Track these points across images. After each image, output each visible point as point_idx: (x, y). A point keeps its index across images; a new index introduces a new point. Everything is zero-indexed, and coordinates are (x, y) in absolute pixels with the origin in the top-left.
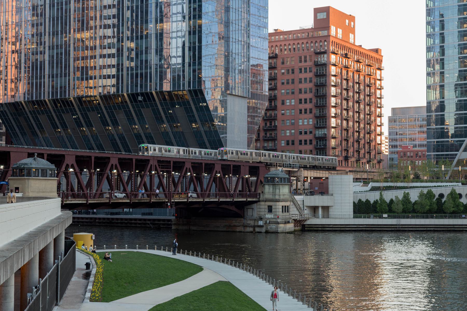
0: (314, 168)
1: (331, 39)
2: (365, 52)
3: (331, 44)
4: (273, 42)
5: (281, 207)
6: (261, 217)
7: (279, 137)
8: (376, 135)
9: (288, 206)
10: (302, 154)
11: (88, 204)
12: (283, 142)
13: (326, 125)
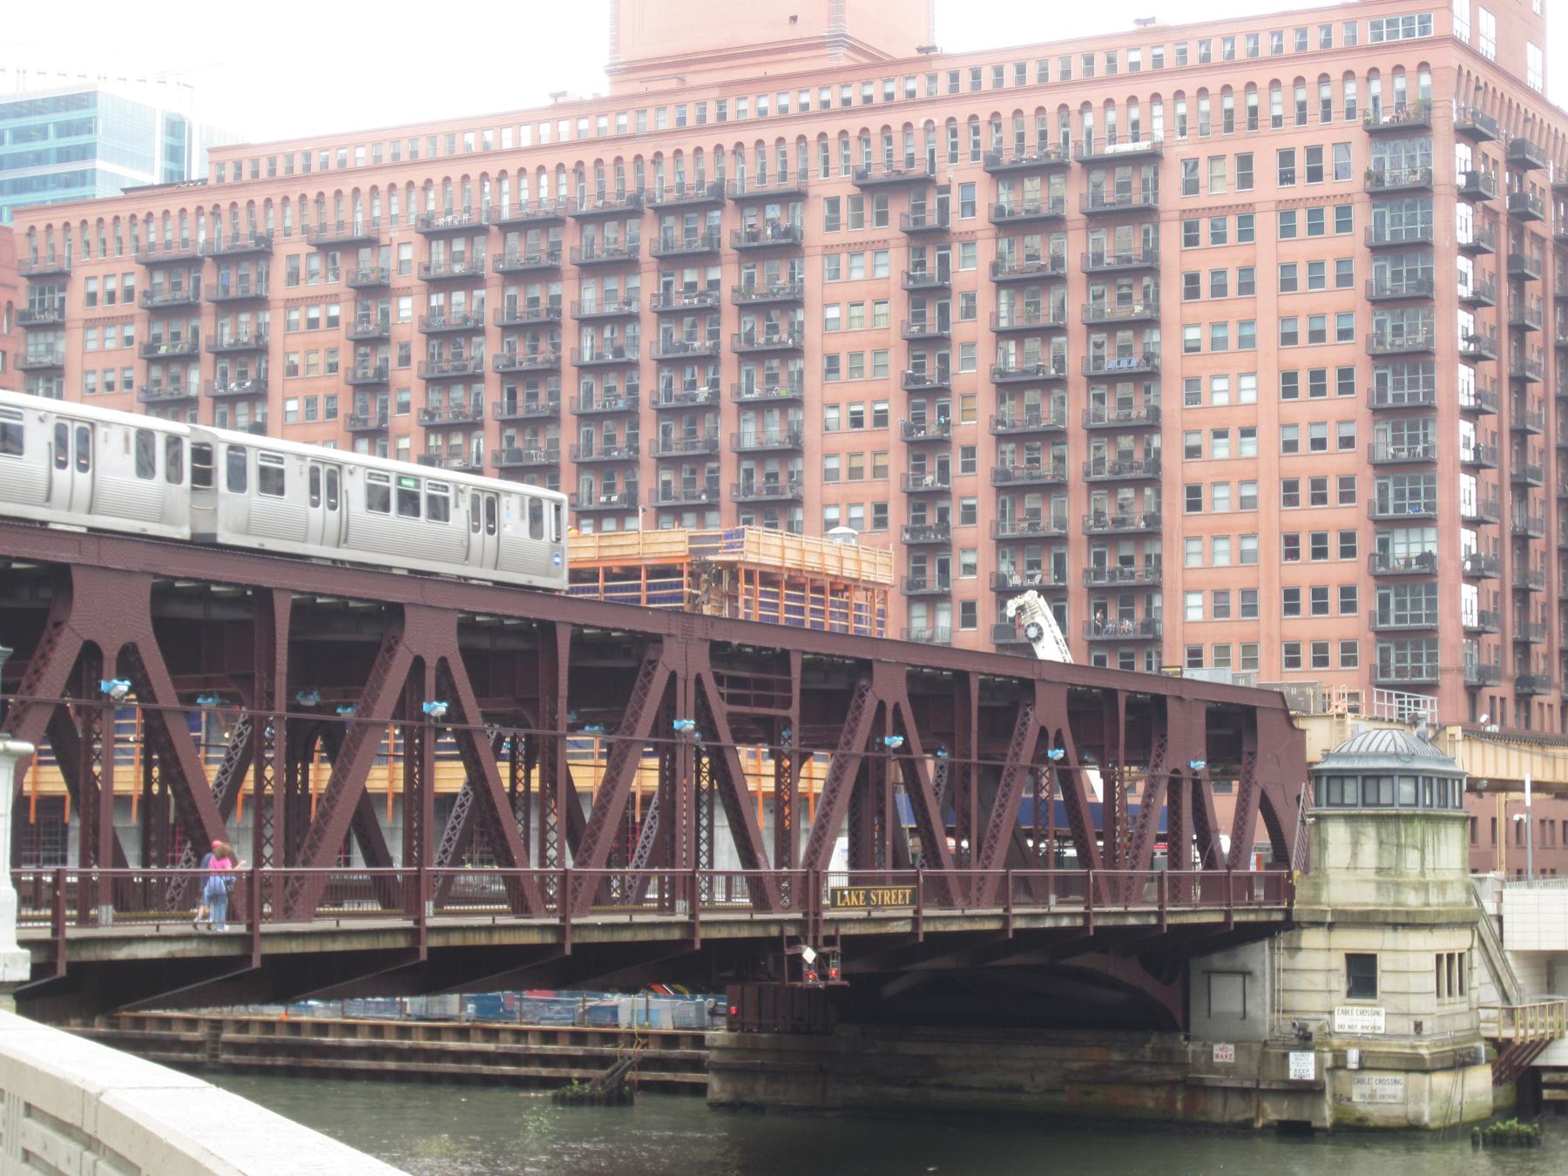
6: (1303, 1028)
7: (1171, 573)
11: (256, 963)
12: (1194, 600)
13: (1431, 507)
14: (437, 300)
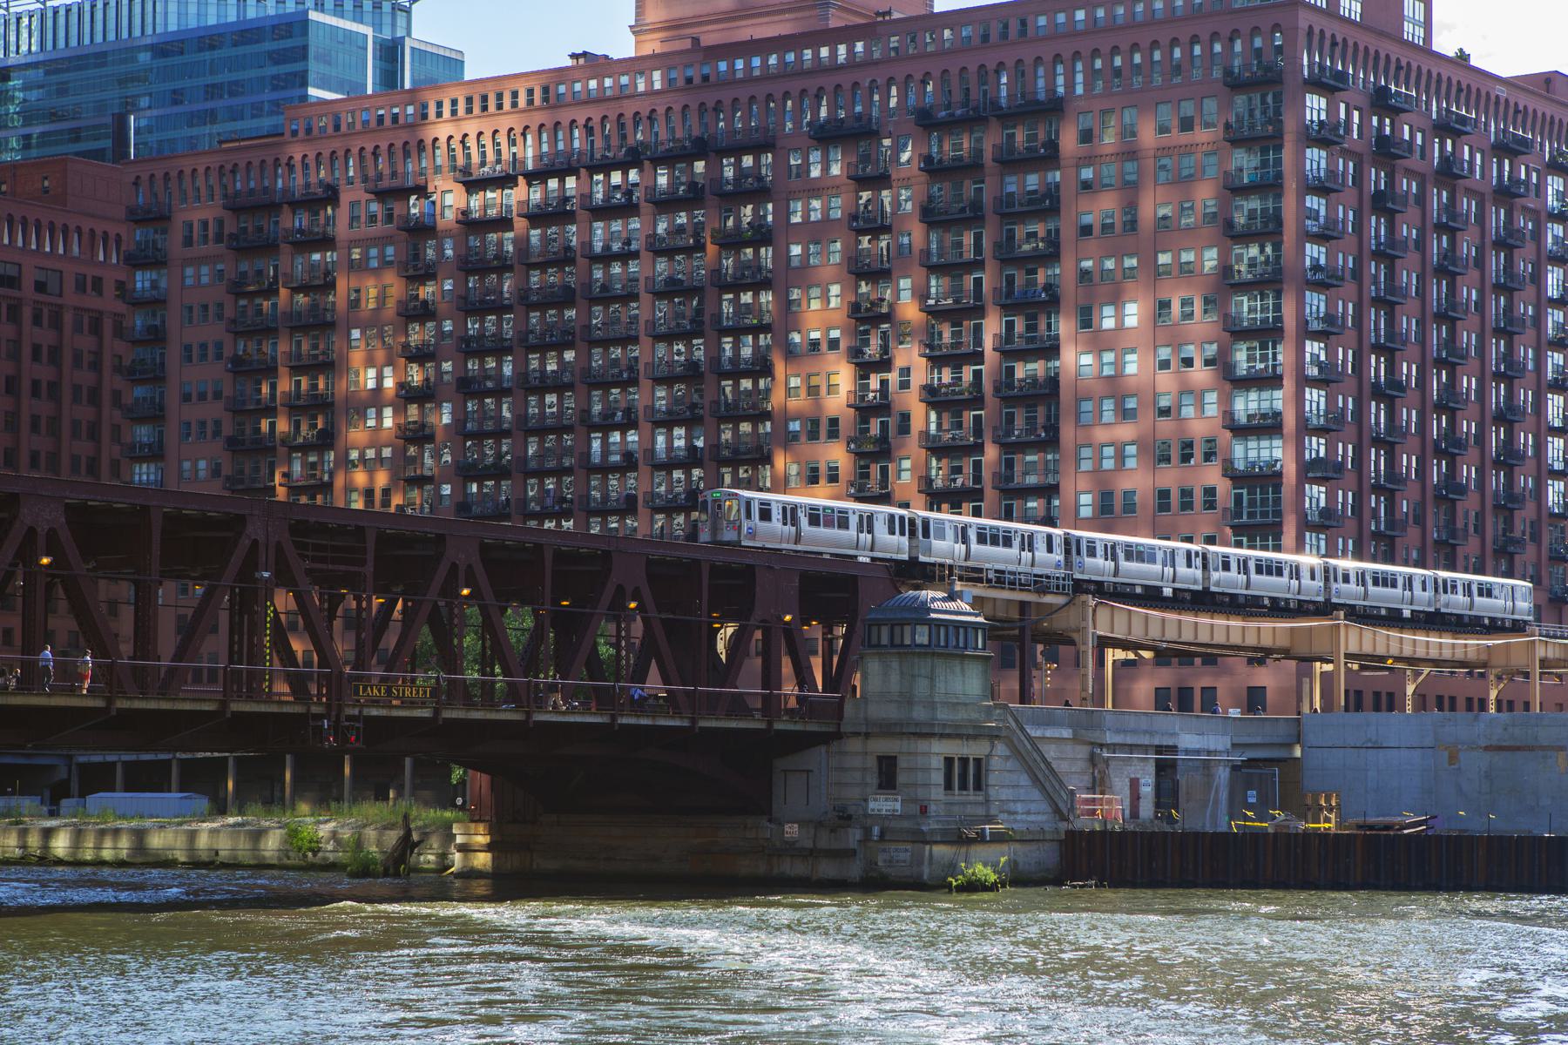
0: (1433, 623)
1: (1304, 20)
2: (1502, 92)
3: (1302, 39)
4: (1044, 39)
5: (937, 763)
8: (1366, 440)
9: (978, 761)
10: (980, 516)
14: (474, 242)
